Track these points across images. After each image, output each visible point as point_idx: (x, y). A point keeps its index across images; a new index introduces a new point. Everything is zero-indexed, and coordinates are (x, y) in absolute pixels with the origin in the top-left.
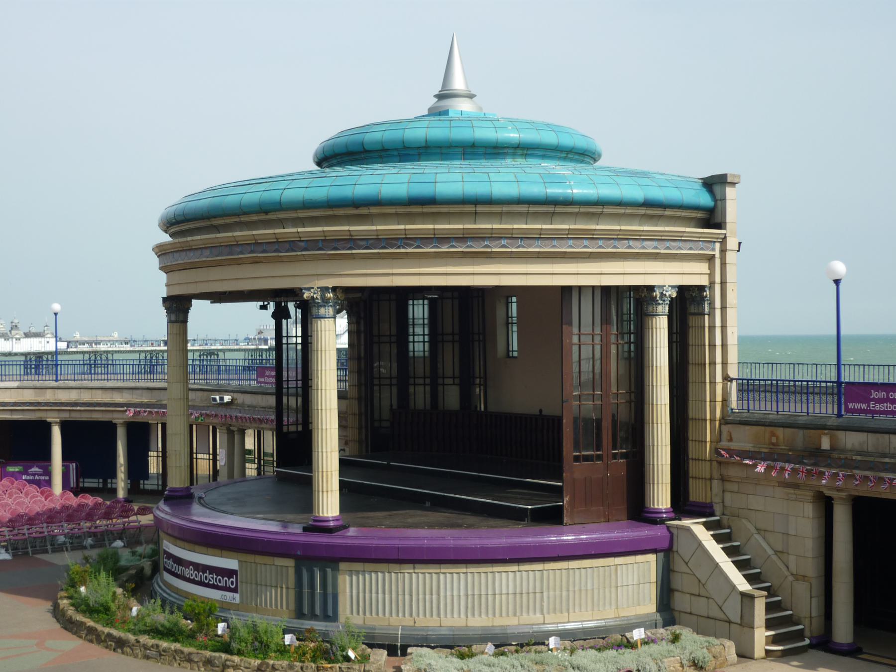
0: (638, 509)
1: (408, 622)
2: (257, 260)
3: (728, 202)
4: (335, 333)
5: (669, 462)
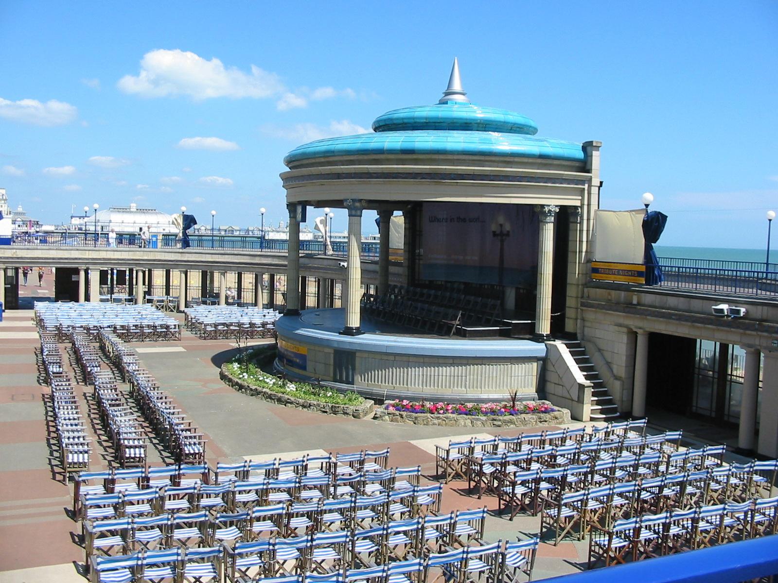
2: (323, 183)
3: (593, 157)
4: (398, 218)
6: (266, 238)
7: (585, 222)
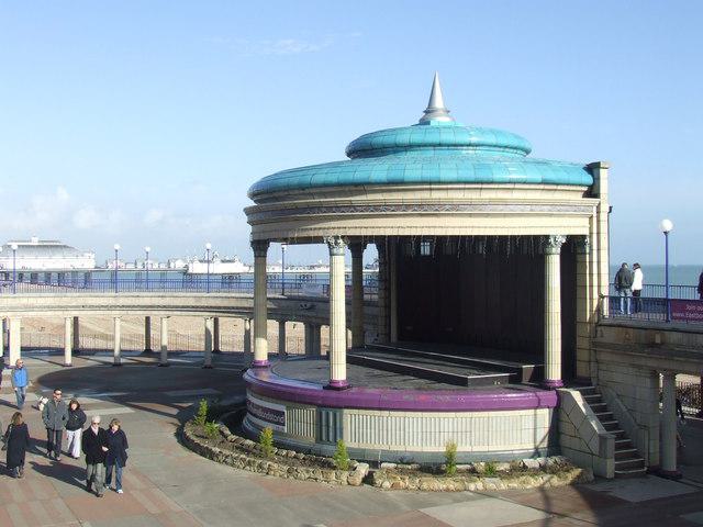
0: (539, 380)
1: (385, 448)
4: (371, 254)
5: (560, 350)
6: (190, 271)
7: (595, 252)
